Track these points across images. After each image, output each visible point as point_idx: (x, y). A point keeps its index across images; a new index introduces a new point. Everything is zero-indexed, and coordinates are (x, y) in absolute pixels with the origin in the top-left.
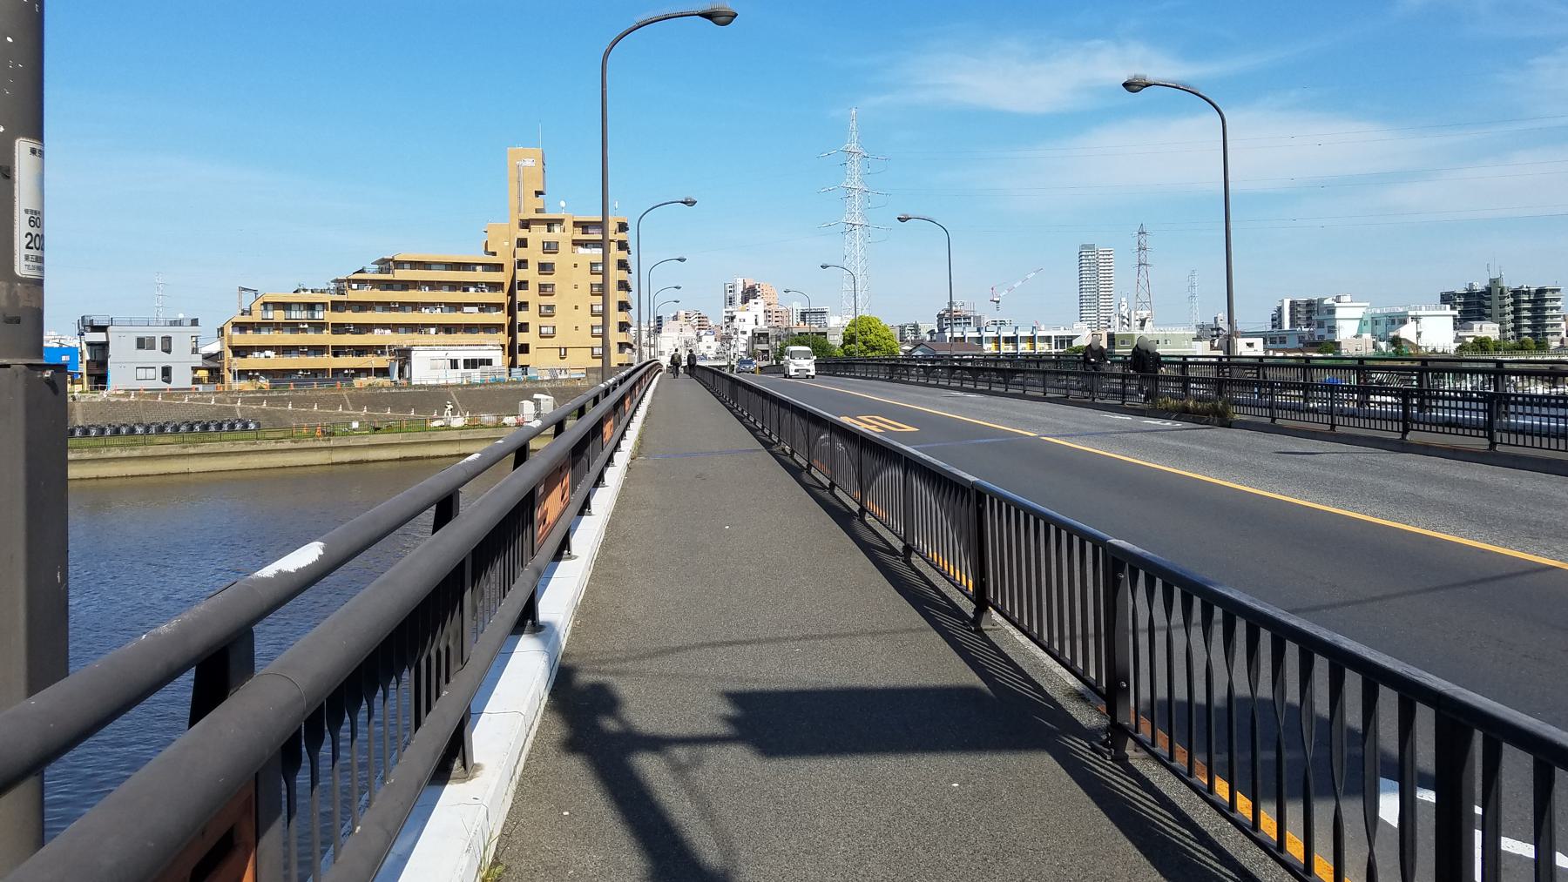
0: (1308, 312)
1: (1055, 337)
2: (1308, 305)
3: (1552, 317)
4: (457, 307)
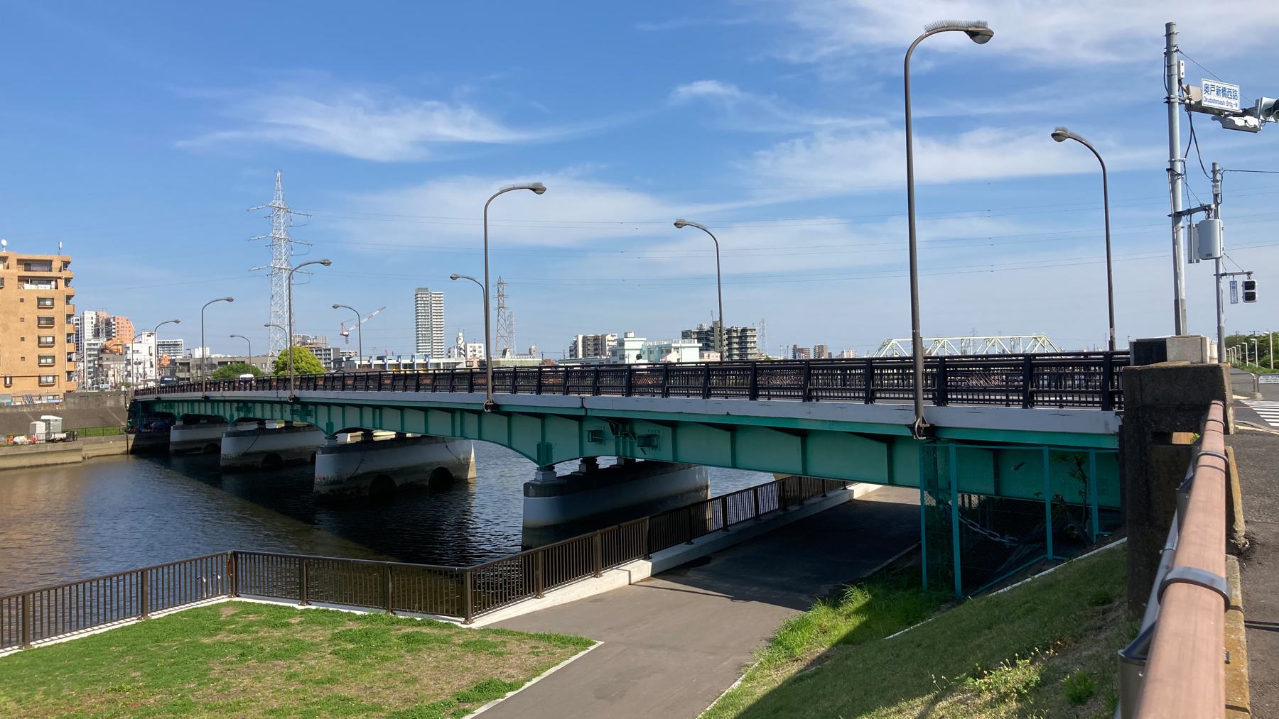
0: (595, 345)
1: (443, 363)
2: (594, 340)
3: (751, 348)
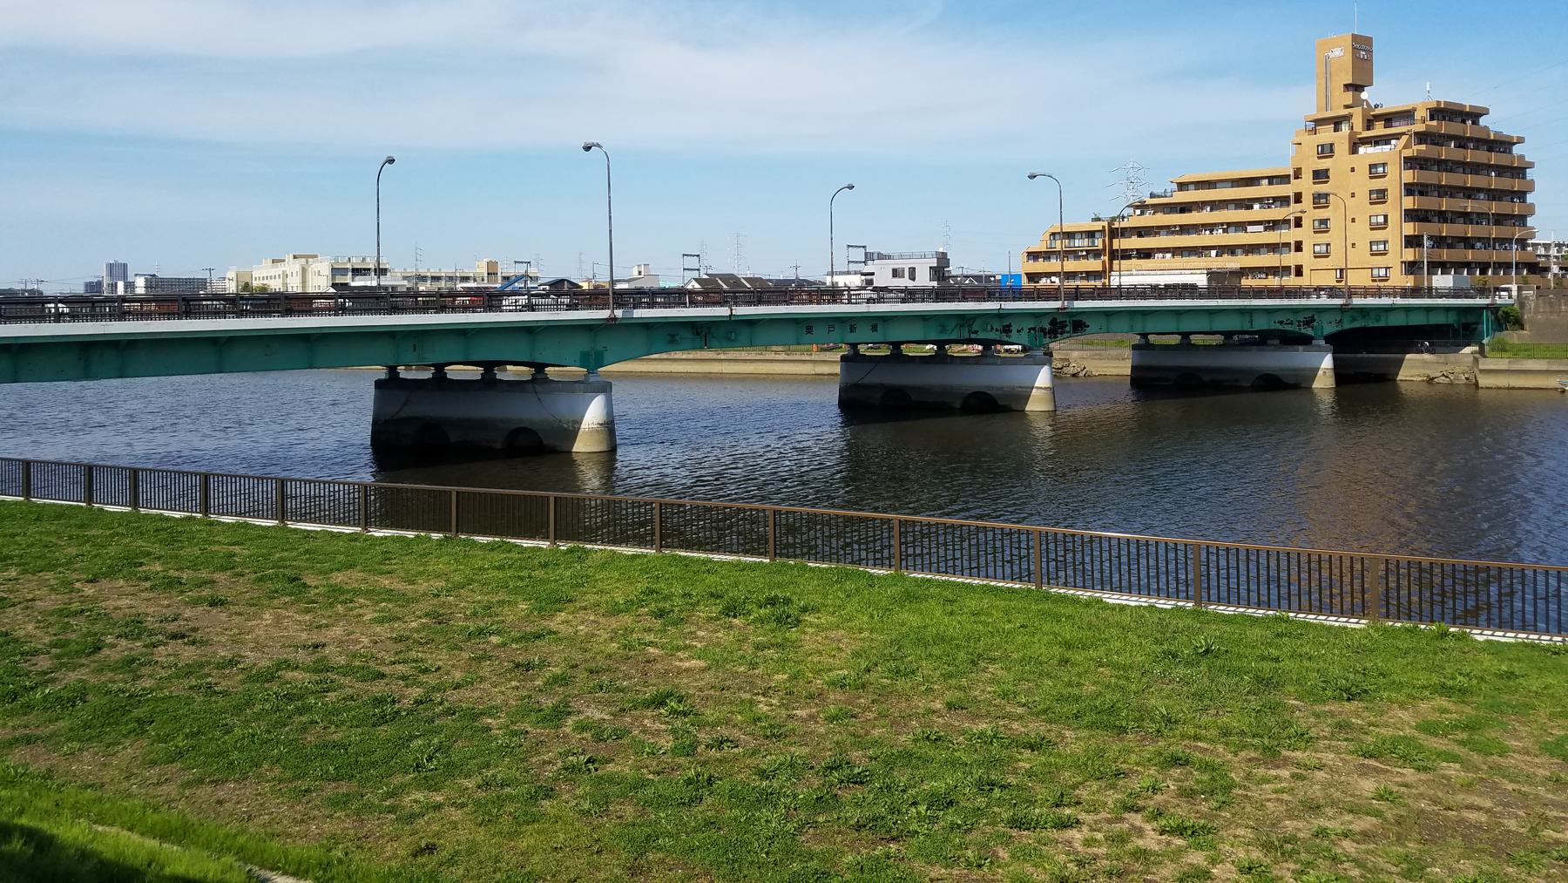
4: (1241, 226)
